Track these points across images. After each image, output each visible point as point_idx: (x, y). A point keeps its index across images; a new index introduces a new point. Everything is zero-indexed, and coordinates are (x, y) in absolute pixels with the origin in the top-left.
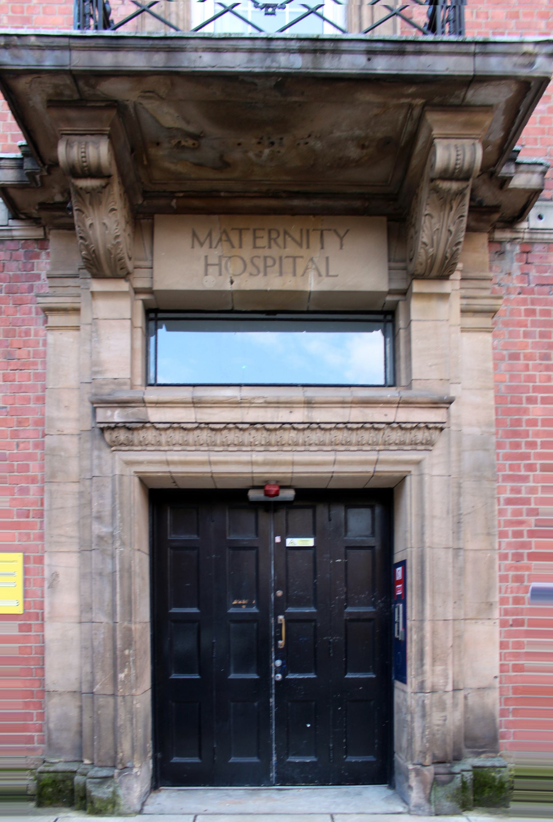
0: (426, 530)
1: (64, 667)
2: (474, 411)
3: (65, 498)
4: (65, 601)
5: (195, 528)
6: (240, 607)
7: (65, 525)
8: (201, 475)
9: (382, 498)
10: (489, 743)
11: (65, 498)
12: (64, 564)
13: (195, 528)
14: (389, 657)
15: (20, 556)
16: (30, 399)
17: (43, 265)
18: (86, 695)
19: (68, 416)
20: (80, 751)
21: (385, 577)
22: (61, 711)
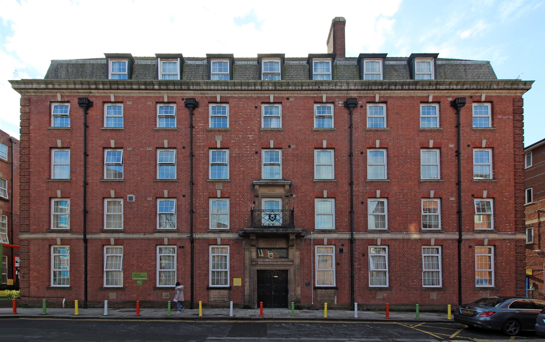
0: (291, 276)
1: (247, 292)
2: (297, 261)
3: (247, 272)
4: (247, 284)
5: (263, 277)
6: (268, 285)
7: (247, 275)
8: (243, 63)
9: (286, 271)
10: (299, 302)
11: (247, 272)
12: (247, 280)
13: (263, 277)
14: (286, 291)
15: (318, 155)
16: (172, 308)
17: (244, 242)
18: (250, 295)
19: (247, 262)
20: (249, 302)
21: (286, 281)
22: (247, 298)
